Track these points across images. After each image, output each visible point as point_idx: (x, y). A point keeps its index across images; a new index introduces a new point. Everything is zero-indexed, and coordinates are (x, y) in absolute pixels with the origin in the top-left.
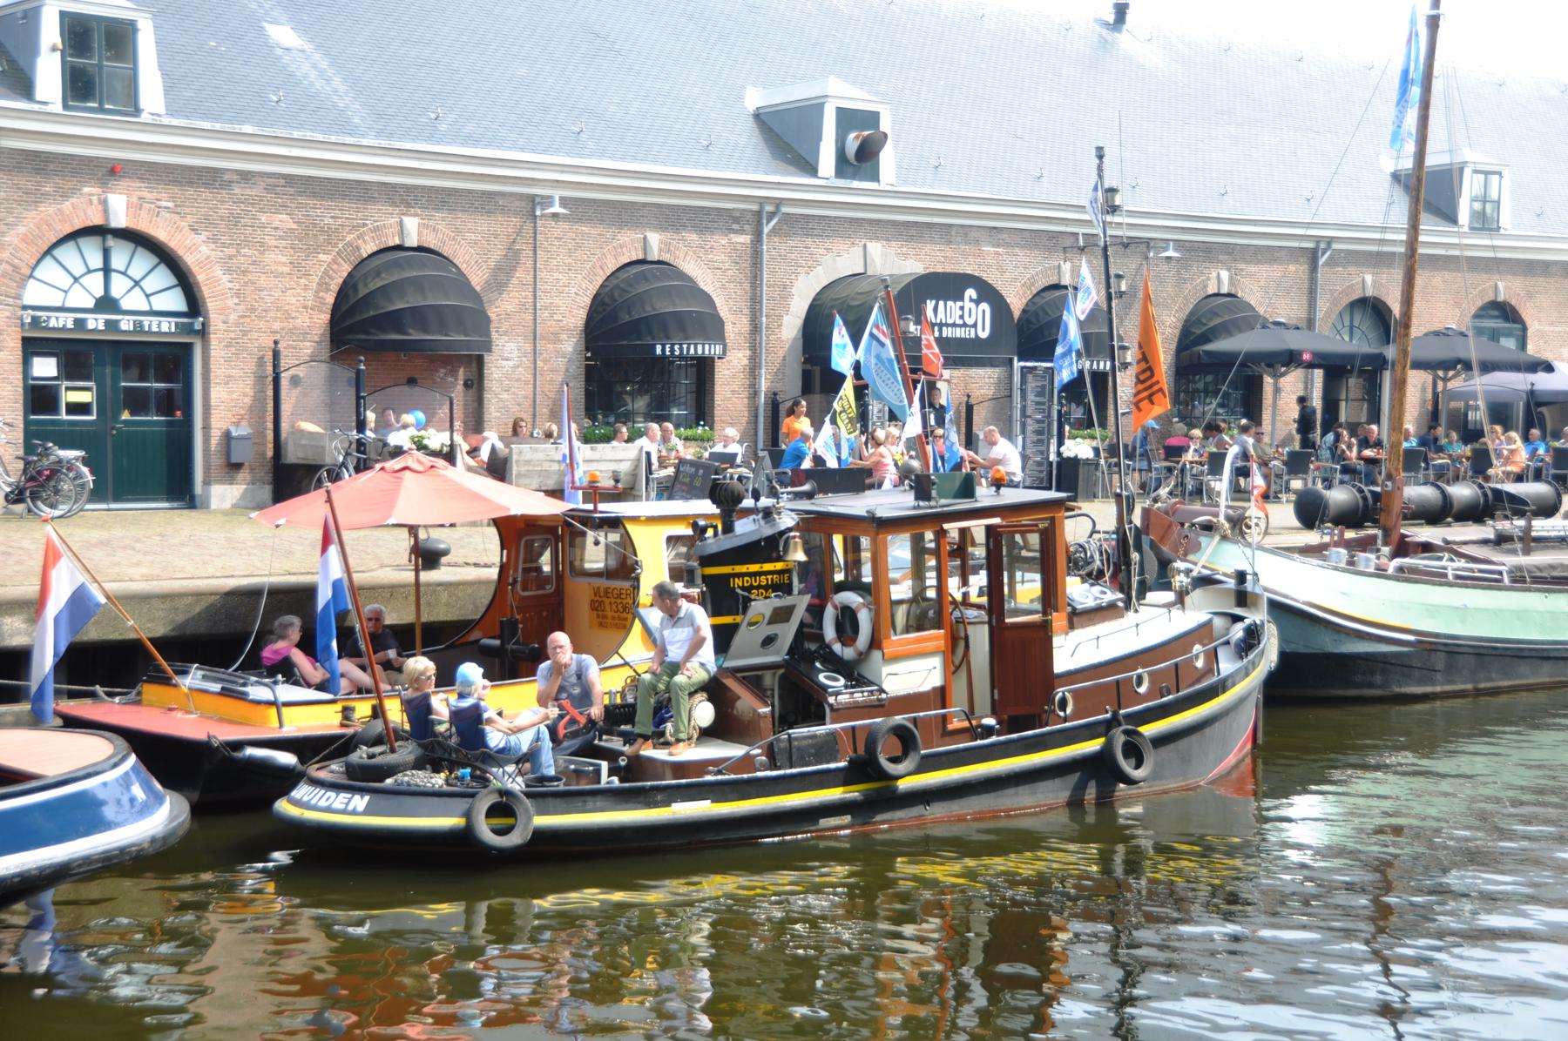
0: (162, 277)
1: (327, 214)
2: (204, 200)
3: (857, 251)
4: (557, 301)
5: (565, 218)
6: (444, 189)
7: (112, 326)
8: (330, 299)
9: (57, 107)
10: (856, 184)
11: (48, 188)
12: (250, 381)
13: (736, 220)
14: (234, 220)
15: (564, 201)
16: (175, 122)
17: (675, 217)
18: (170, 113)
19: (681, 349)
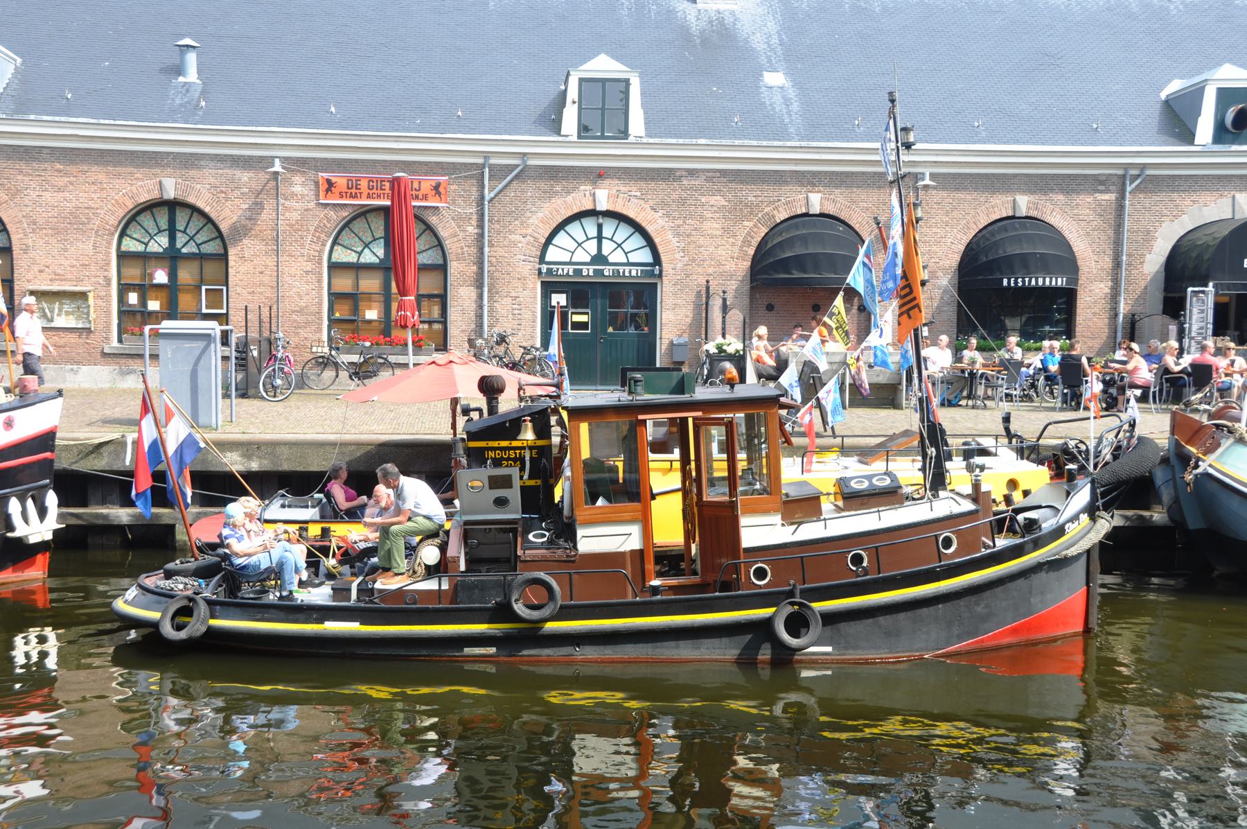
0: (637, 241)
1: (751, 194)
2: (661, 190)
3: (1226, 202)
4: (934, 248)
5: (934, 188)
6: (842, 173)
7: (599, 273)
8: (751, 252)
9: (575, 138)
10: (1235, 148)
11: (558, 188)
12: (691, 307)
13: (1102, 183)
14: (682, 202)
15: (933, 176)
16: (651, 141)
17: (1041, 183)
18: (648, 135)
19: (1024, 282)
